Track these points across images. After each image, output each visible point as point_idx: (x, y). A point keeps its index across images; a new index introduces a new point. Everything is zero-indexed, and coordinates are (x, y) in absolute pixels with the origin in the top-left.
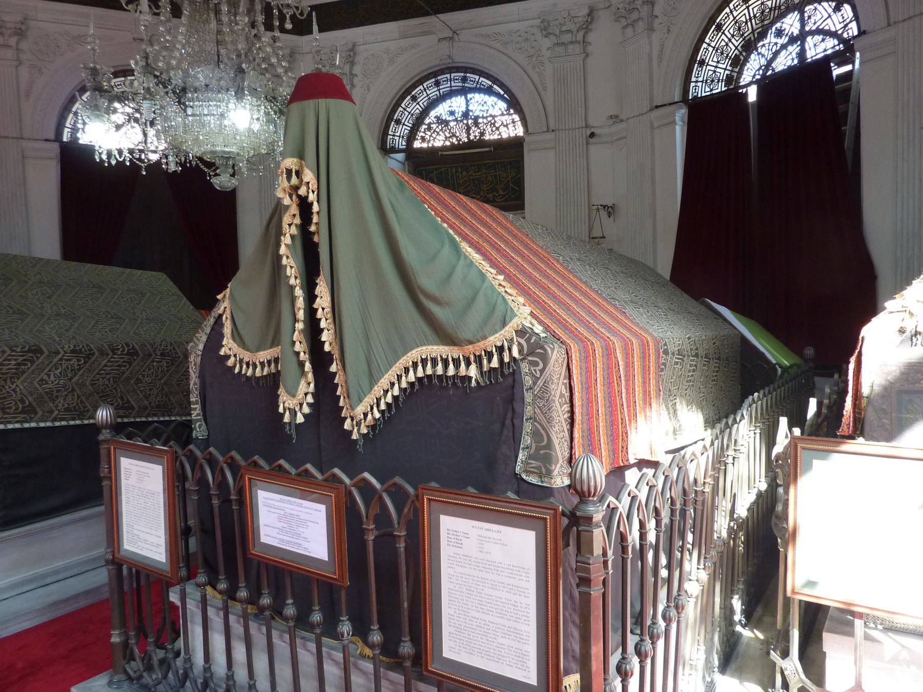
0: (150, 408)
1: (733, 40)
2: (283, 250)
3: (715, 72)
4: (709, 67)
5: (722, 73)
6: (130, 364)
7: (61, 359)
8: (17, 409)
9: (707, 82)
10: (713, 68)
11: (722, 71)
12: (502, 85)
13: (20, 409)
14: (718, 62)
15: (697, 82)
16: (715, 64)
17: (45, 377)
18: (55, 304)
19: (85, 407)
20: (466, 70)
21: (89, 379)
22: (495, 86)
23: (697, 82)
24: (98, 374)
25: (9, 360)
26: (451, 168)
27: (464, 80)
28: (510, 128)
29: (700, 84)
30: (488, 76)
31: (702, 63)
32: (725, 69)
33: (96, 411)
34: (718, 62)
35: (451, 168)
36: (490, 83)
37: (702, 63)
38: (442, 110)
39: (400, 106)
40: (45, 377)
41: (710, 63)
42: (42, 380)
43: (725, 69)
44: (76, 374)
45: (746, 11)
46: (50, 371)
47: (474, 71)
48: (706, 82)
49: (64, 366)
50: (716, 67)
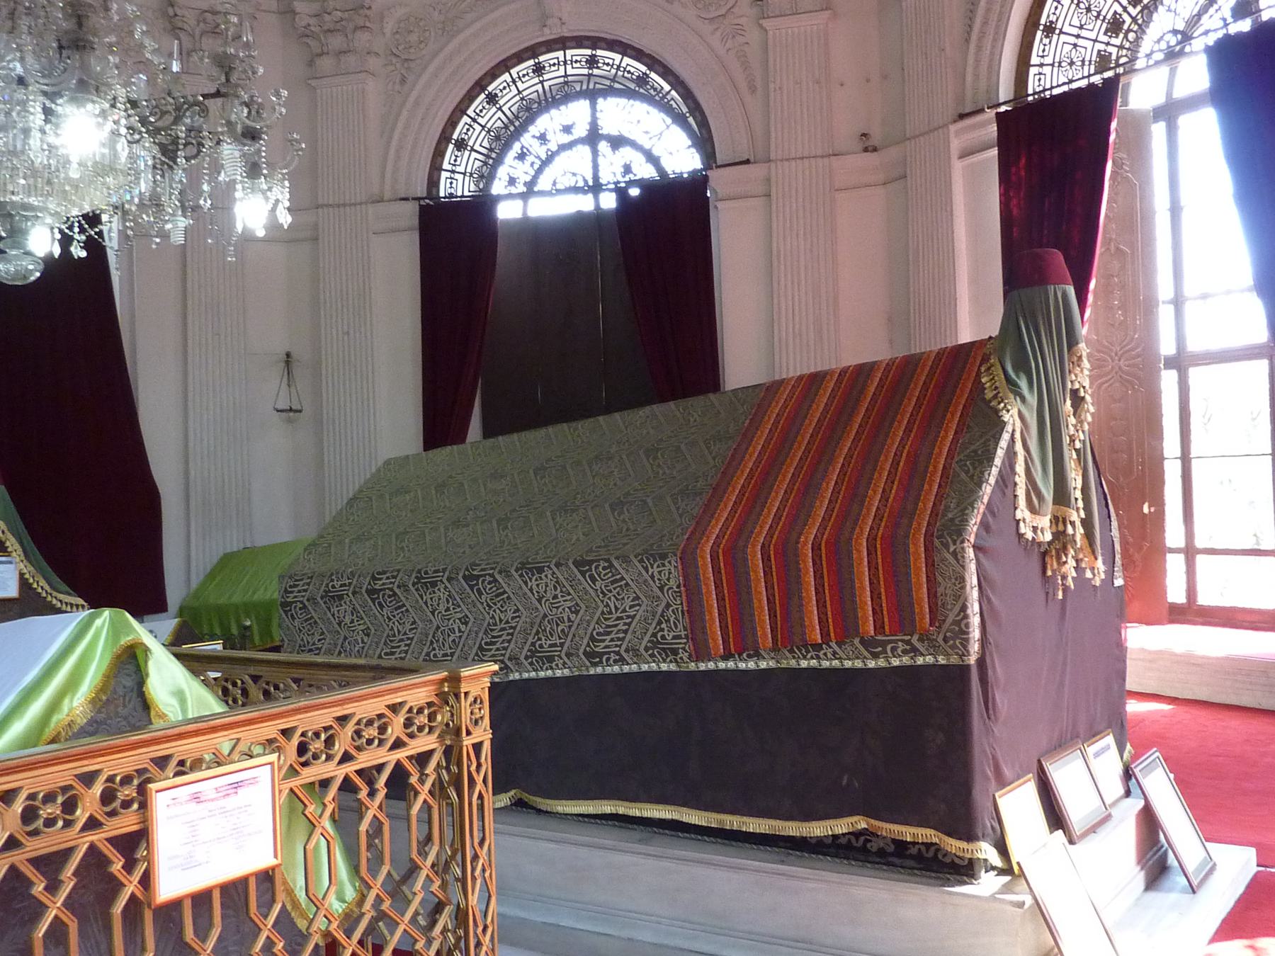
1: (1084, 33)
5: (1089, 51)
6: (592, 638)
9: (457, 183)
11: (1089, 44)
12: (666, 73)
14: (1081, 27)
15: (1041, 65)
19: (521, 575)
20: (594, 42)
21: (523, 618)
22: (653, 75)
24: (633, 617)
25: (619, 639)
27: (592, 62)
28: (681, 158)
29: (1047, 70)
30: (639, 55)
31: (1050, 30)
32: (1095, 41)
36: (644, 68)
37: (1050, 30)
38: (549, 122)
39: (440, 169)
40: (573, 617)
42: (577, 612)
43: (1095, 41)
44: (662, 616)
46: (570, 627)
47: (613, 45)
49: (555, 636)
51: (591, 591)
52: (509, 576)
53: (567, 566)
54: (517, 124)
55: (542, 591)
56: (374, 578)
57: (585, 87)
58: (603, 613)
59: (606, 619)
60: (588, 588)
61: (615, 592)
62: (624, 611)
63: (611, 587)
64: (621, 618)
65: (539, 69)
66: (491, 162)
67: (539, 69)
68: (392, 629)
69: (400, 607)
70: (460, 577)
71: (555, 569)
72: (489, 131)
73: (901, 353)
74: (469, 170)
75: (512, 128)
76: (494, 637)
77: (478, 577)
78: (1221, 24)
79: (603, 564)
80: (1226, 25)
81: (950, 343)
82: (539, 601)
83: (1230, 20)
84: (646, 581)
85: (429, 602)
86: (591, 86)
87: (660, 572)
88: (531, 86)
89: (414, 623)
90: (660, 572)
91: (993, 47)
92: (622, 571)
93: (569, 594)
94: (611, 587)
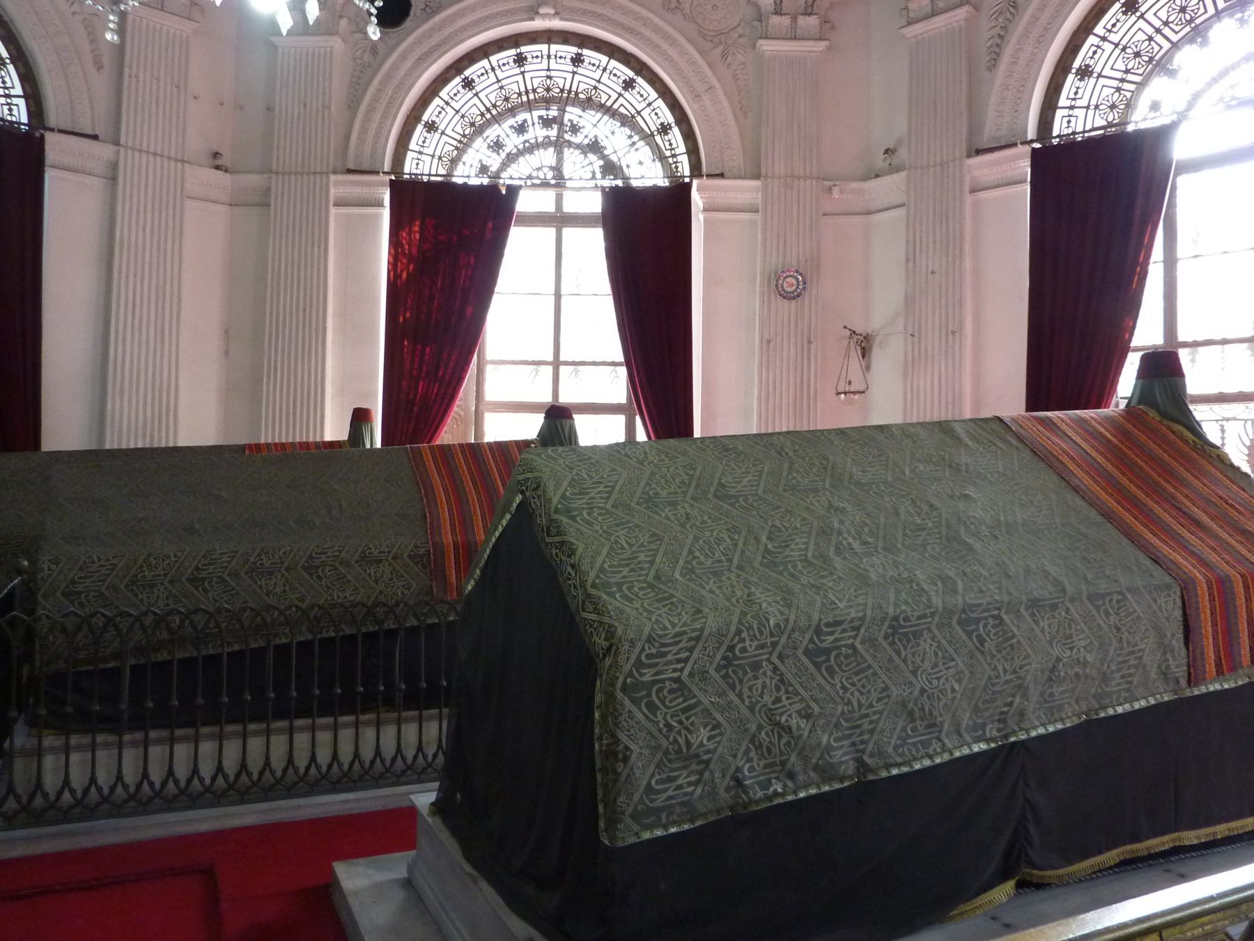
0: (283, 570)
2: (964, 537)
3: (1150, 39)
4: (1141, 23)
7: (166, 575)
8: (660, 690)
10: (1150, 31)
13: (654, 689)
14: (1166, 23)
15: (1104, 39)
16: (1158, 24)
17: (53, 567)
18: (642, 463)
23: (1104, 39)
26: (1087, 637)
29: (1108, 47)
33: (366, 33)
34: (1166, 23)
35: (1087, 637)
41: (1149, 16)
42: (57, 564)
45: (615, 96)
48: (1124, 49)
50: (1158, 31)
51: (828, 688)
52: (1019, 616)
53: (950, 625)
54: (531, 96)
55: (918, 660)
56: (818, 631)
57: (609, 104)
58: (990, 678)
59: (993, 685)
60: (823, 682)
61: (859, 685)
62: (871, 706)
63: (855, 679)
64: (1133, 652)
65: (629, 85)
66: (488, 116)
67: (629, 85)
68: (995, 669)
69: (862, 671)
70: (954, 623)
71: (937, 633)
72: (501, 88)
73: (240, 438)
74: (463, 111)
75: (525, 98)
76: (994, 693)
77: (978, 620)
78: (590, 175)
79: (1115, 597)
80: (594, 177)
81: (298, 436)
82: (914, 673)
83: (599, 175)
84: (1155, 612)
85: (910, 658)
86: (615, 106)
87: (1050, 626)
88: (610, 89)
89: (886, 688)
90: (914, 654)
91: (395, 93)
92: (698, 693)
93: (1083, 632)
94: (855, 679)
